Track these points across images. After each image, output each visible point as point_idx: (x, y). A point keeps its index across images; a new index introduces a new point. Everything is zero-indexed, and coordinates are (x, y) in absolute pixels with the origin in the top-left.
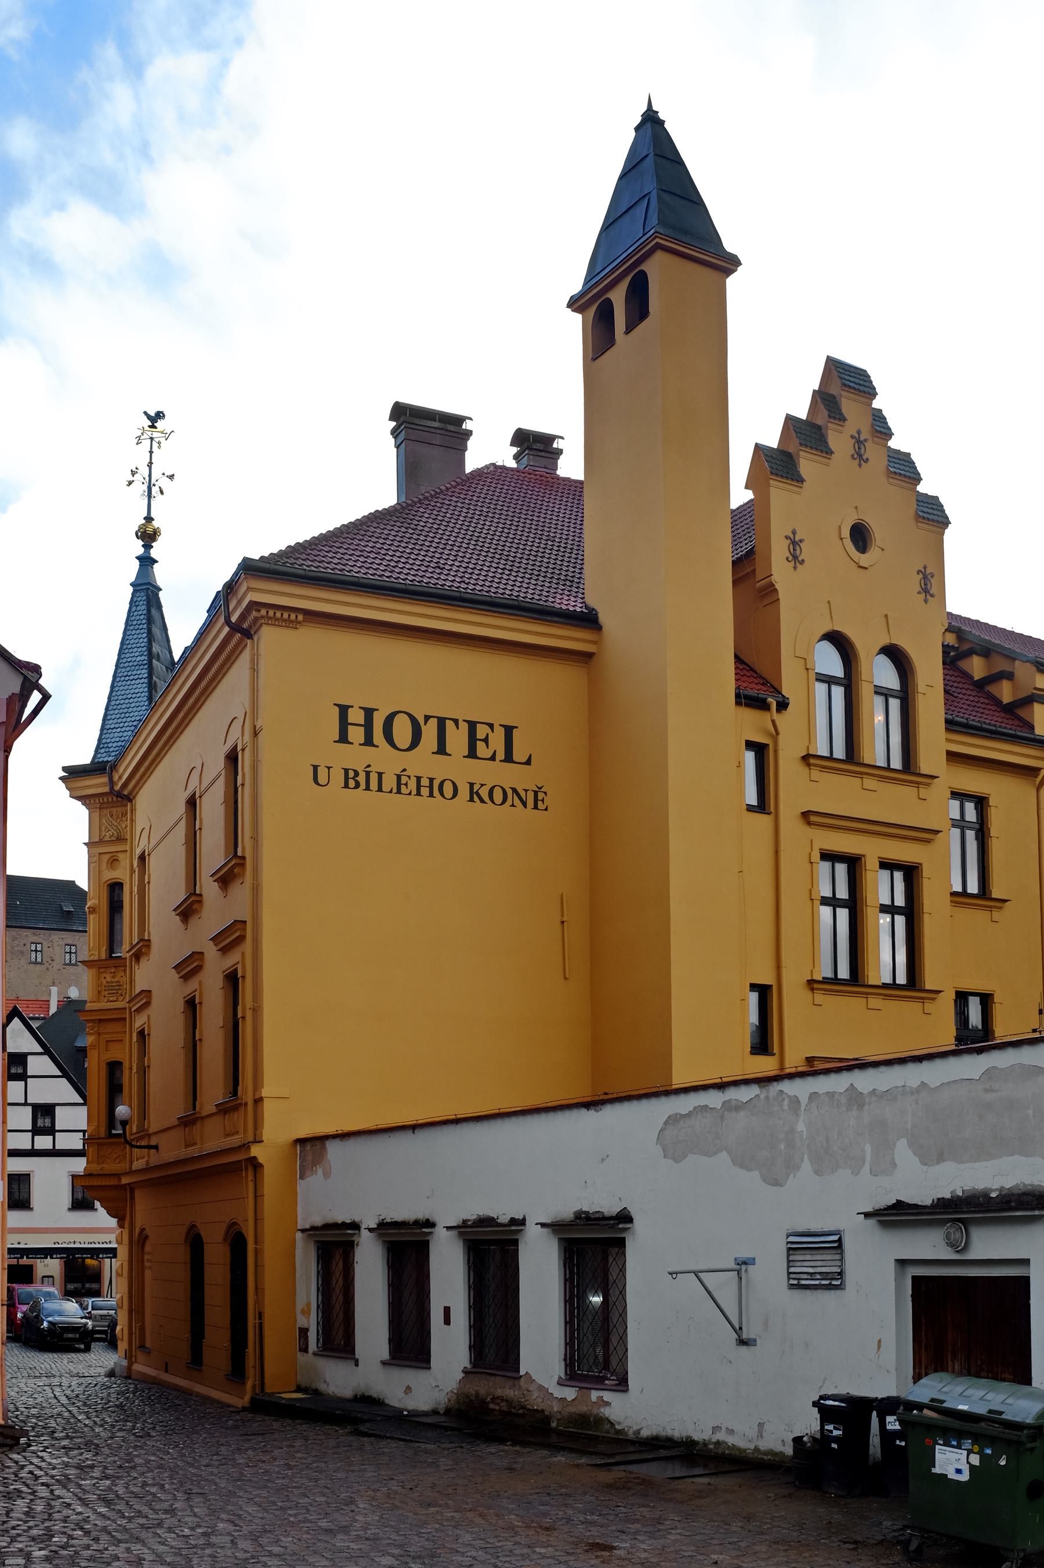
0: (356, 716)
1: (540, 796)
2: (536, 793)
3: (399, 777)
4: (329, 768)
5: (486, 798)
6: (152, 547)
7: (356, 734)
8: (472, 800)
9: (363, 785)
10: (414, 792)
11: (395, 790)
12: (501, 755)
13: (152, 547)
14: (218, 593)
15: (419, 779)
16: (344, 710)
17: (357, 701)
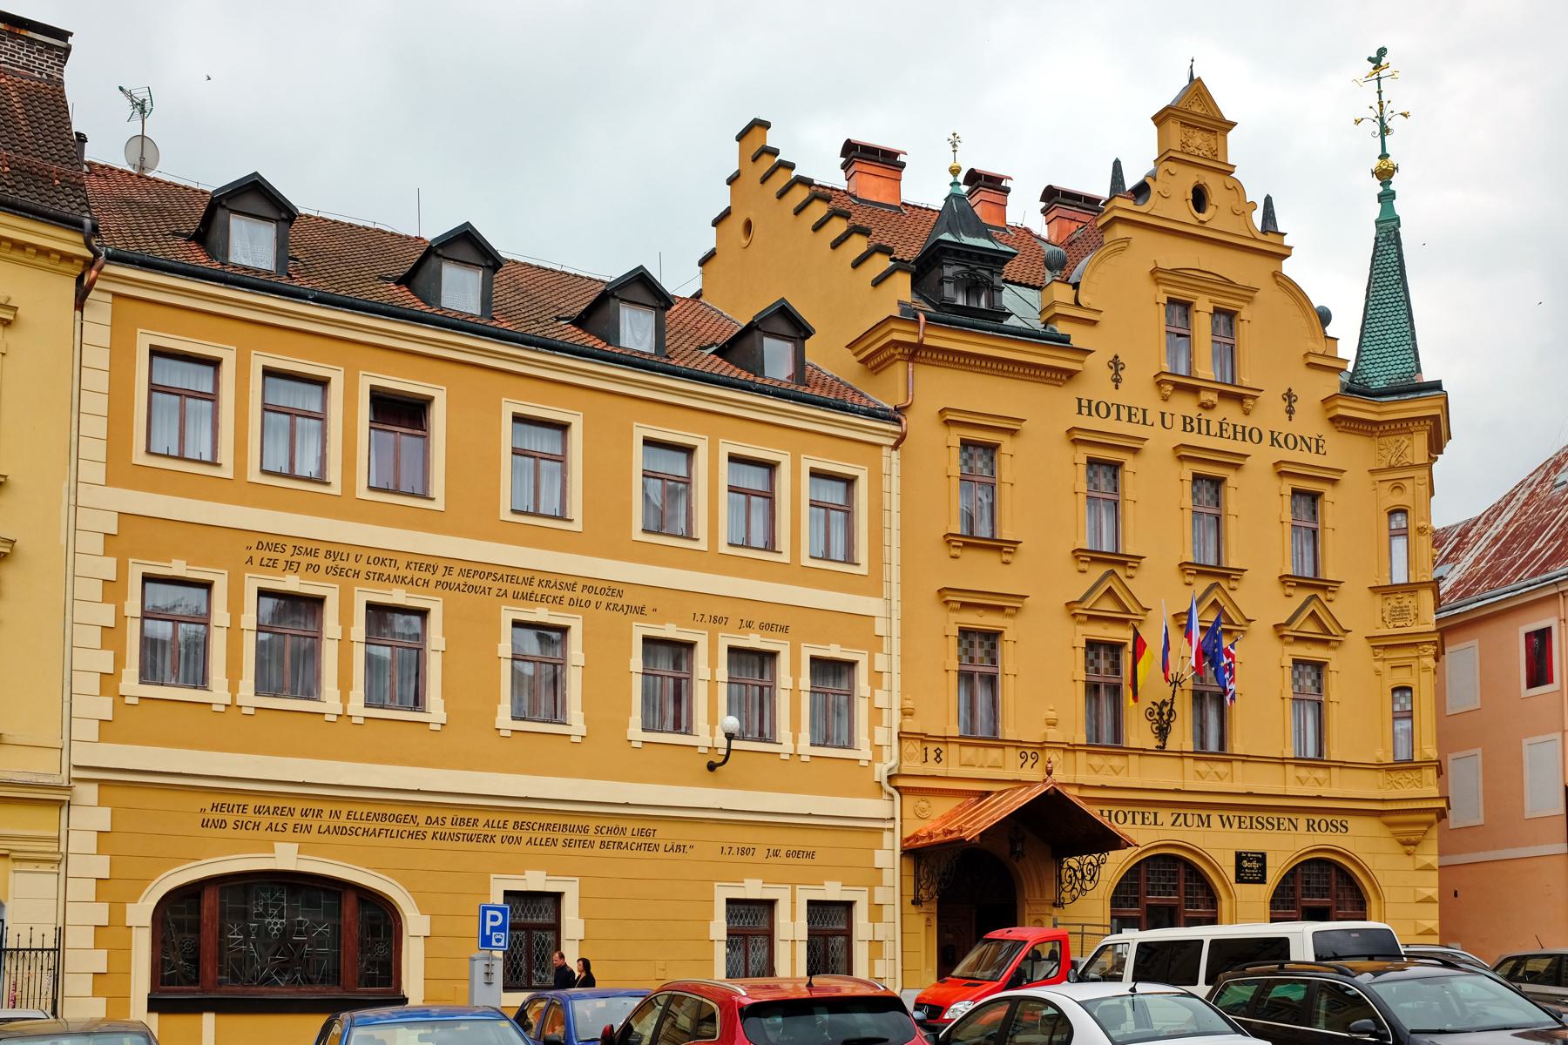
0: (1085, 403)
1: (1321, 443)
2: (1317, 440)
3: (1221, 424)
4: (1172, 415)
7: (1085, 411)
8: (1272, 445)
10: (1232, 437)
11: (1218, 435)
12: (1141, 422)
13: (1391, 182)
14: (1399, 226)
15: (1235, 426)
16: (1080, 400)
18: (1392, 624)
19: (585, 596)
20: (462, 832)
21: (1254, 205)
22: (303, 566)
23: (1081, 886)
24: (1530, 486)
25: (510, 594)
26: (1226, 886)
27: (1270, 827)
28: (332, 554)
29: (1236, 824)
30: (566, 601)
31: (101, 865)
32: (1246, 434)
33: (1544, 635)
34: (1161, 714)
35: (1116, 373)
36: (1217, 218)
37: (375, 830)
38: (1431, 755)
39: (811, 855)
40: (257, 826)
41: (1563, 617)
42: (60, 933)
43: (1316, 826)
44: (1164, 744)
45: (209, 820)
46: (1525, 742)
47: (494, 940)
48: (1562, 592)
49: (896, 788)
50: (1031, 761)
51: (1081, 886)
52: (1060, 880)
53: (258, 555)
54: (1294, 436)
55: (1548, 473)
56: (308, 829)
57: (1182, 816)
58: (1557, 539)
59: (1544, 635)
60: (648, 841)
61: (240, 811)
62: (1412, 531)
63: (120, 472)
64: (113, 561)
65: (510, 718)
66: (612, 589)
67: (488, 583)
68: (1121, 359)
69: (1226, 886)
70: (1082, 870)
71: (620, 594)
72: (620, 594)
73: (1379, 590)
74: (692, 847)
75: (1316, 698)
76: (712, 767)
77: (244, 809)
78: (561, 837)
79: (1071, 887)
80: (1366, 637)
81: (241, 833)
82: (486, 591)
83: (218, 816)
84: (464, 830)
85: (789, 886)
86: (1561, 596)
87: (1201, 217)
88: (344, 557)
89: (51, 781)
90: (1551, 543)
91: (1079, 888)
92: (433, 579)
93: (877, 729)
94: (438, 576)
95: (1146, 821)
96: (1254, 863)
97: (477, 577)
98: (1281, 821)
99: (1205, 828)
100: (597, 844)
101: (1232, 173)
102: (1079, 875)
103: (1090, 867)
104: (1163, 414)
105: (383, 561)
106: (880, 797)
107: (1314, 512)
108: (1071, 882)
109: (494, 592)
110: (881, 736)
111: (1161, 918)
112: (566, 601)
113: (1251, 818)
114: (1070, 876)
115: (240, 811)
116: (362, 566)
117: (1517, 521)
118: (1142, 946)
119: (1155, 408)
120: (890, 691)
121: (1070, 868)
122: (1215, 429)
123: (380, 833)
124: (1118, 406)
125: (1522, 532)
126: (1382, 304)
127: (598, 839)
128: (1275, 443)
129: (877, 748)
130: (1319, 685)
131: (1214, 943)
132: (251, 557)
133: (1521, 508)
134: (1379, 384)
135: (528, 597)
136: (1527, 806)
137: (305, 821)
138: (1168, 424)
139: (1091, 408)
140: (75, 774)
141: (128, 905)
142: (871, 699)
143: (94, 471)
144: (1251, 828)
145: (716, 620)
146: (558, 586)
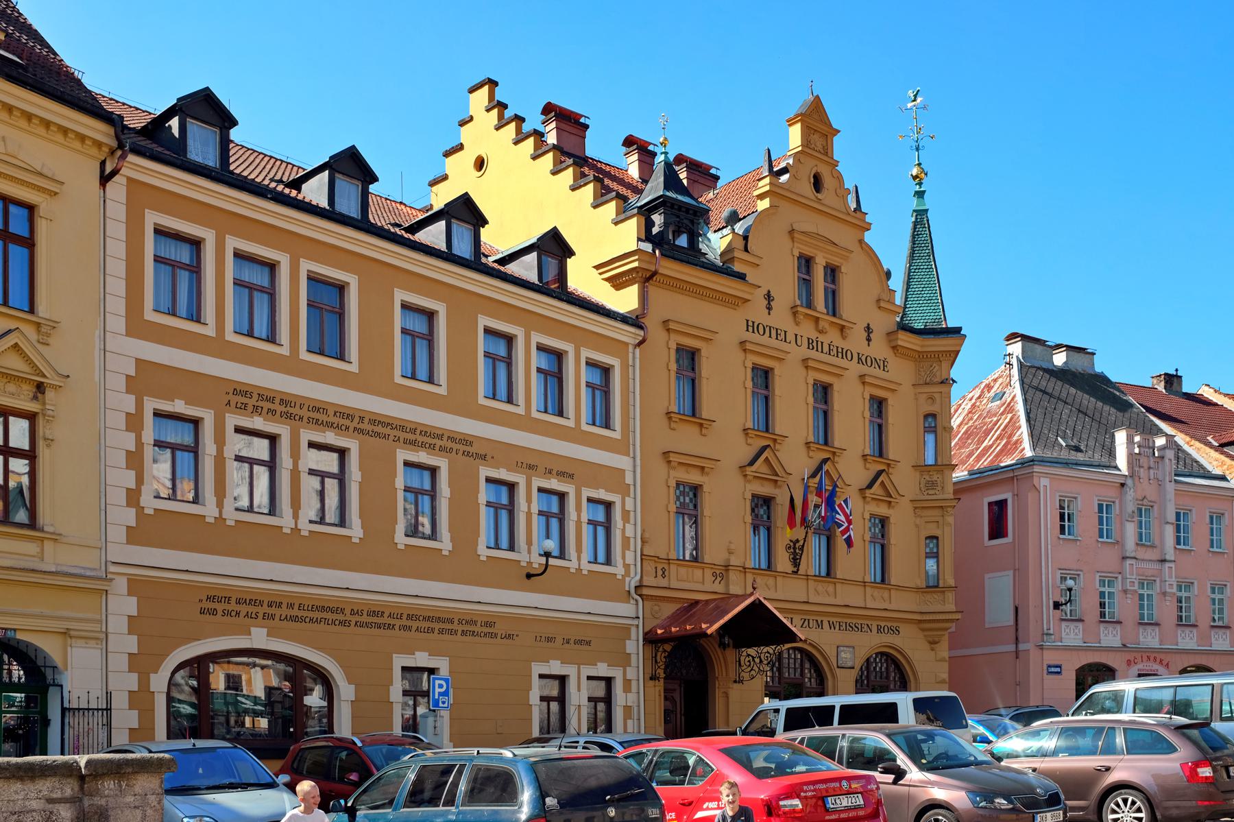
0: (750, 324)
1: (886, 363)
2: (884, 361)
3: (830, 345)
7: (751, 329)
8: (858, 363)
12: (784, 340)
15: (837, 347)
16: (747, 321)
17: (751, 319)
18: (926, 492)
19: (449, 444)
20: (374, 621)
21: (848, 190)
22: (265, 410)
23: (759, 669)
24: (971, 399)
25: (402, 440)
26: (831, 670)
27: (857, 630)
28: (284, 402)
29: (837, 627)
30: (437, 448)
31: (132, 643)
32: (843, 353)
33: (1002, 504)
34: (795, 548)
35: (769, 303)
36: (827, 196)
37: (287, 616)
38: (951, 583)
39: (588, 643)
40: (238, 614)
41: (1016, 493)
42: (109, 696)
43: (882, 630)
44: (798, 570)
45: (205, 609)
46: (987, 576)
47: (440, 703)
48: (1016, 476)
49: (640, 595)
50: (719, 579)
51: (759, 669)
52: (740, 665)
53: (235, 399)
54: (758, 332)
55: (982, 392)
56: (273, 617)
57: (807, 621)
58: (1002, 439)
59: (1002, 504)
60: (491, 630)
61: (226, 601)
62: (939, 430)
63: (137, 327)
64: (133, 397)
65: (538, 555)
66: (466, 440)
67: (387, 431)
68: (772, 294)
69: (831, 670)
70: (760, 657)
71: (471, 444)
72: (471, 444)
73: (919, 468)
74: (517, 636)
75: (882, 541)
76: (529, 576)
77: (229, 600)
78: (437, 626)
79: (750, 669)
80: (911, 501)
81: (227, 619)
82: (386, 437)
83: (211, 605)
84: (375, 620)
85: (576, 666)
86: (1015, 478)
87: (819, 196)
88: (293, 405)
89: (95, 574)
90: (998, 441)
91: (757, 670)
92: (352, 425)
93: (627, 552)
94: (355, 424)
95: (842, 628)
96: (848, 654)
97: (380, 426)
98: (863, 626)
99: (820, 630)
100: (460, 632)
101: (837, 166)
102: (757, 660)
103: (767, 654)
104: (796, 335)
105: (318, 410)
106: (628, 602)
107: (880, 412)
108: (750, 665)
109: (391, 438)
110: (630, 557)
111: (797, 691)
112: (437, 448)
113: (846, 623)
114: (749, 661)
115: (226, 601)
116: (305, 413)
117: (966, 424)
118: (789, 711)
119: (792, 330)
120: (635, 525)
121: (749, 655)
122: (826, 349)
123: (320, 621)
124: (770, 327)
125: (972, 432)
126: (920, 269)
127: (460, 628)
128: (860, 362)
129: (627, 566)
130: (695, 501)
131: (843, 707)
132: (229, 401)
133: (967, 415)
134: (919, 325)
135: (413, 443)
136: (987, 619)
137: (409, 623)
138: (799, 343)
139: (751, 326)
140: (112, 569)
141: (151, 675)
142: (624, 530)
143: (117, 323)
144: (846, 630)
145: (531, 467)
146: (432, 436)
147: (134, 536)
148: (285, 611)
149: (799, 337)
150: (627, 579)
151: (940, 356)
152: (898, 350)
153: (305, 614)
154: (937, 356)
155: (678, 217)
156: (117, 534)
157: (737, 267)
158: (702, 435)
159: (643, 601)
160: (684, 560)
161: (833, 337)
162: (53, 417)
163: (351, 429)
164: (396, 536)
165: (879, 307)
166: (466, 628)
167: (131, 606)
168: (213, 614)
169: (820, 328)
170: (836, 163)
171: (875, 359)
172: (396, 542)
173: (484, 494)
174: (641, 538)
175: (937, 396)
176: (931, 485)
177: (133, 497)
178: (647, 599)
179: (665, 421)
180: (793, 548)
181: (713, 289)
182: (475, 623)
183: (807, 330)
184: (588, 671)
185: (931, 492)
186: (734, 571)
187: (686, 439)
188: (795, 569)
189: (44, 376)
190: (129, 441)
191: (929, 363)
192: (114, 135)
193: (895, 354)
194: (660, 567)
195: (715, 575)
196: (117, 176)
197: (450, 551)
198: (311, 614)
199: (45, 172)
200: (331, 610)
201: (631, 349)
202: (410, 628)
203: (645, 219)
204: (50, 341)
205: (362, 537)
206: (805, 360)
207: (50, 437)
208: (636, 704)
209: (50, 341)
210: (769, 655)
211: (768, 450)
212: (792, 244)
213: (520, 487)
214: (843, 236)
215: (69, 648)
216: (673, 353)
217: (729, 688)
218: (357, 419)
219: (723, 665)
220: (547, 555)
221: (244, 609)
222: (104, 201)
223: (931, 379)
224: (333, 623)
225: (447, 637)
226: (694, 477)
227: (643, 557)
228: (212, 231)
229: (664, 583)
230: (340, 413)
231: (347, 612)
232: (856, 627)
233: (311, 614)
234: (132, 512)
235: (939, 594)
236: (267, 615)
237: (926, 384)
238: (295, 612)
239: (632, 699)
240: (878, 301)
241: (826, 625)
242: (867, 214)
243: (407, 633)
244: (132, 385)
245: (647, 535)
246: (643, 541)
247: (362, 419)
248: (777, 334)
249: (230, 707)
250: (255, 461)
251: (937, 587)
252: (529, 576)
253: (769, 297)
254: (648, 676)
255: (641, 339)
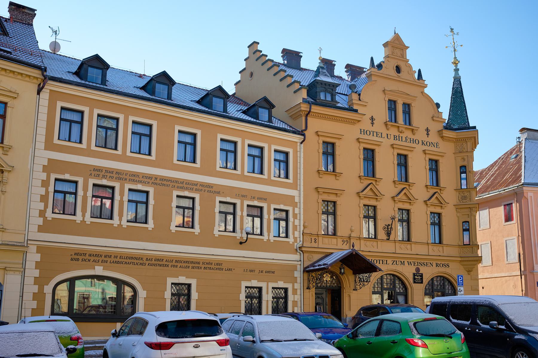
0: (362, 130)
1: (438, 144)
2: (437, 144)
3: (406, 138)
4: (390, 135)
5: (426, 144)
6: (457, 66)
7: (362, 133)
9: (398, 139)
10: (409, 142)
11: (405, 141)
12: (381, 137)
15: (410, 139)
16: (361, 130)
17: (362, 129)
18: (462, 201)
19: (201, 188)
22: (108, 177)
27: (424, 265)
30: (194, 189)
31: (37, 273)
32: (414, 141)
39: (273, 272)
40: (89, 260)
43: (439, 265)
44: (389, 238)
45: (73, 258)
49: (302, 251)
50: (346, 243)
52: (356, 282)
53: (93, 173)
62: (467, 172)
63: (49, 146)
64: (46, 174)
66: (210, 186)
68: (374, 117)
70: (363, 278)
72: (212, 187)
74: (234, 269)
76: (241, 243)
78: (191, 265)
79: (359, 284)
80: (454, 205)
83: (76, 257)
84: (159, 263)
87: (399, 75)
88: (122, 174)
91: (362, 284)
93: (295, 232)
94: (153, 180)
95: (428, 265)
98: (428, 263)
103: (366, 277)
104: (387, 134)
109: (171, 186)
110: (297, 234)
113: (418, 262)
116: (128, 177)
119: (385, 132)
122: (404, 139)
124: (373, 132)
127: (203, 266)
129: (295, 239)
138: (389, 137)
139: (365, 132)
142: (294, 222)
145: (243, 196)
147: (41, 229)
148: (112, 259)
149: (389, 135)
150: (296, 244)
151: (466, 139)
152: (444, 138)
153: (123, 260)
154: (464, 140)
155: (325, 88)
156: (34, 228)
157: (355, 107)
158: (336, 179)
159: (303, 253)
160: (328, 235)
161: (408, 134)
162: (6, 183)
163: (150, 183)
164: (214, 231)
165: (433, 120)
166: (206, 266)
167: (38, 257)
168: (77, 261)
169: (400, 130)
170: (408, 61)
171: (432, 143)
172: (214, 234)
173: (218, 208)
174: (303, 226)
175: (466, 157)
176: (464, 198)
177: (42, 213)
178: (306, 253)
179: (317, 174)
180: (387, 228)
181: (325, 114)
182: (212, 264)
183: (393, 131)
184: (272, 285)
185: (464, 201)
186: (353, 239)
187: (329, 182)
188: (388, 238)
189: (3, 167)
190: (43, 191)
191: (461, 143)
192: (41, 74)
193: (443, 140)
194: (313, 238)
195: (343, 241)
196: (44, 89)
197: (293, 242)
198: (125, 260)
199: (12, 90)
200: (136, 259)
201: (299, 144)
202: (177, 266)
203: (307, 91)
204: (8, 153)
205: (199, 232)
206: (392, 145)
207: (4, 191)
208: (299, 300)
209: (8, 153)
210: (367, 278)
211: (437, 193)
212: (385, 96)
213: (238, 205)
214: (412, 91)
215: (6, 275)
216: (396, 157)
217: (351, 293)
218: (154, 179)
219: (347, 281)
220: (248, 234)
221: (92, 258)
222: (39, 99)
223: (462, 150)
224: (137, 264)
225: (196, 270)
226: (332, 198)
227: (304, 234)
228: (87, 107)
229: (316, 245)
230: (145, 176)
231: (145, 259)
232: (423, 264)
233: (125, 260)
234: (41, 219)
235: (470, 248)
236: (104, 261)
237: (460, 152)
238: (118, 259)
239: (297, 298)
240: (433, 117)
241: (406, 263)
242: (425, 80)
243: (175, 268)
244: (45, 169)
245: (306, 224)
246: (304, 227)
247: (156, 179)
248: (377, 134)
249: (85, 300)
250: (255, 216)
251: (469, 245)
252: (241, 243)
253: (372, 119)
254: (305, 287)
255: (303, 140)
